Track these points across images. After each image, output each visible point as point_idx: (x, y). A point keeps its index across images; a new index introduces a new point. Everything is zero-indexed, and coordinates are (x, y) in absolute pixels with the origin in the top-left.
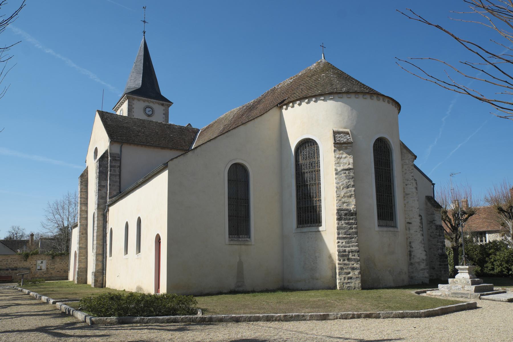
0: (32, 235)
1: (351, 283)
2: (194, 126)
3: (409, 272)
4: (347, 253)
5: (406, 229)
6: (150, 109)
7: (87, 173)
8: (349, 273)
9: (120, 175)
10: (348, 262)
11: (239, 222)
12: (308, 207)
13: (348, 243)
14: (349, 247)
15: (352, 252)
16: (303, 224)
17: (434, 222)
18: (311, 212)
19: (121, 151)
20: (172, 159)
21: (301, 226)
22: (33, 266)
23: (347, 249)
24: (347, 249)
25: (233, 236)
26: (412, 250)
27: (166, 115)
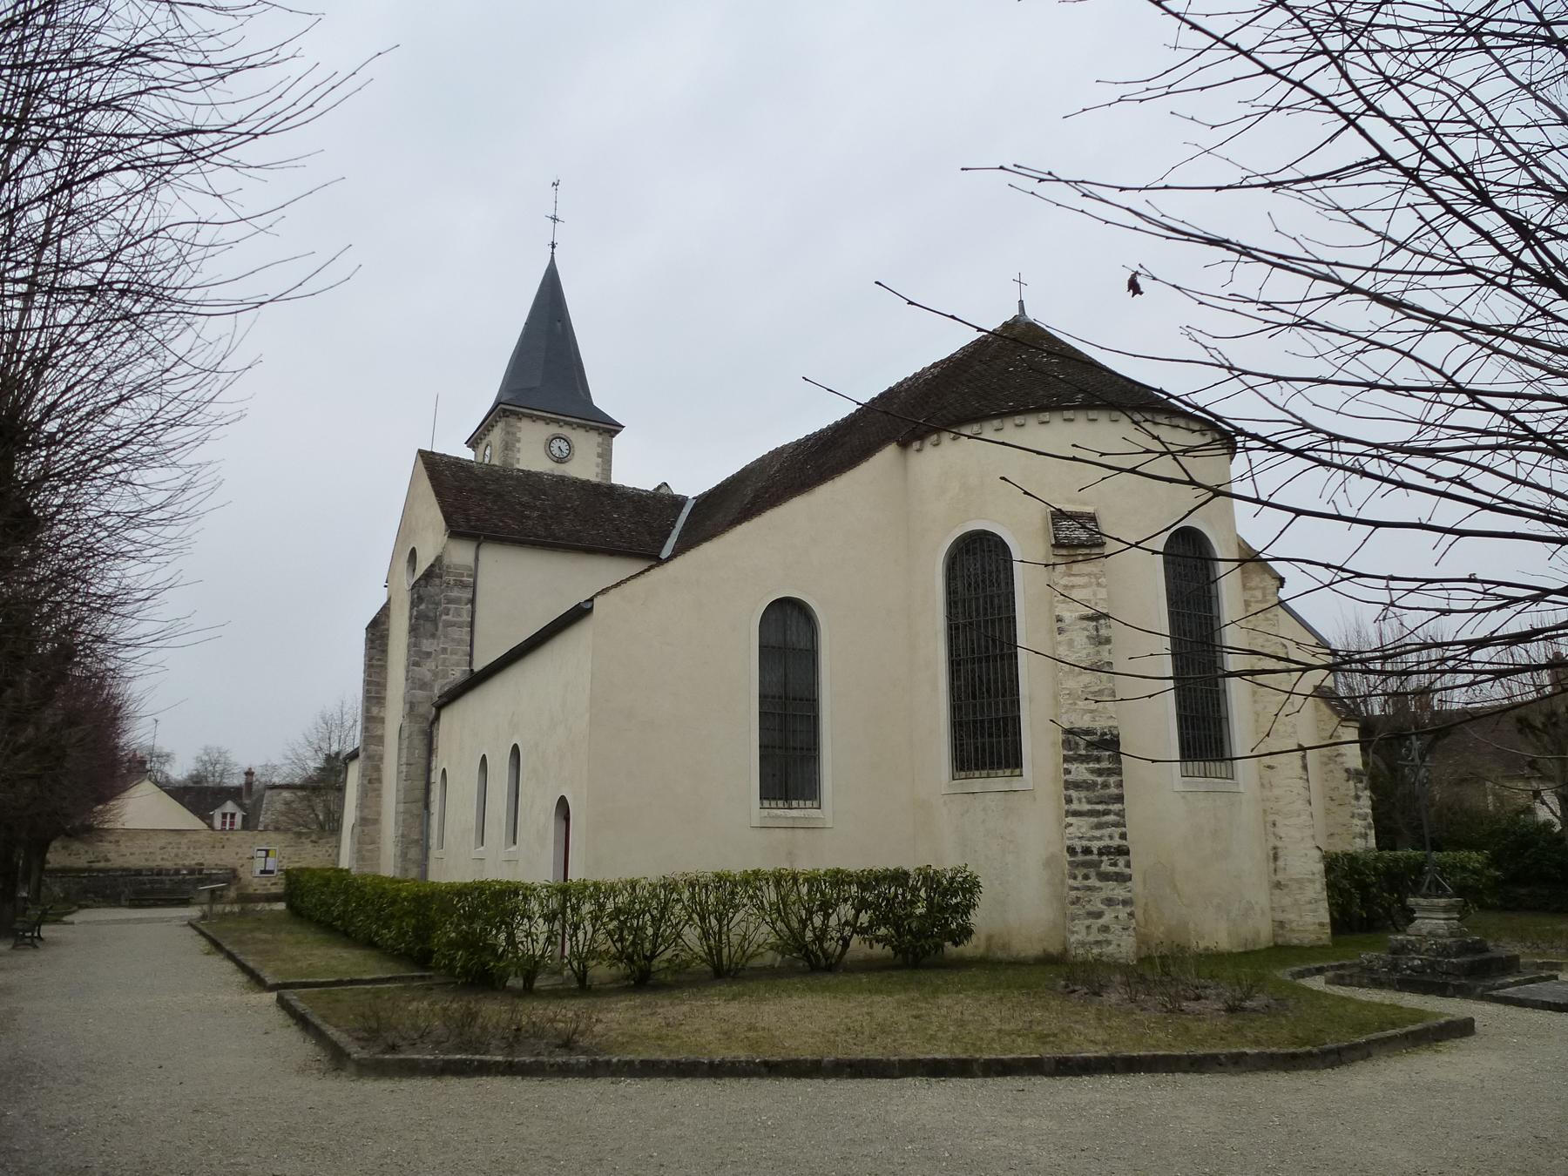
0: (249, 773)
1: (1109, 943)
2: (677, 490)
3: (1273, 909)
4: (1095, 857)
5: (1262, 785)
6: (564, 446)
7: (388, 616)
8: (1099, 915)
9: (472, 624)
10: (1098, 884)
11: (789, 758)
12: (982, 722)
13: (1099, 826)
14: (1100, 838)
15: (1109, 853)
16: (969, 769)
17: (1339, 759)
18: (990, 735)
19: (477, 559)
20: (604, 591)
21: (963, 774)
22: (244, 861)
23: (1095, 845)
24: (1095, 845)
25: (773, 804)
26: (1279, 844)
27: (606, 457)
